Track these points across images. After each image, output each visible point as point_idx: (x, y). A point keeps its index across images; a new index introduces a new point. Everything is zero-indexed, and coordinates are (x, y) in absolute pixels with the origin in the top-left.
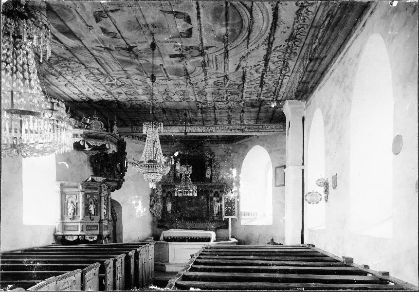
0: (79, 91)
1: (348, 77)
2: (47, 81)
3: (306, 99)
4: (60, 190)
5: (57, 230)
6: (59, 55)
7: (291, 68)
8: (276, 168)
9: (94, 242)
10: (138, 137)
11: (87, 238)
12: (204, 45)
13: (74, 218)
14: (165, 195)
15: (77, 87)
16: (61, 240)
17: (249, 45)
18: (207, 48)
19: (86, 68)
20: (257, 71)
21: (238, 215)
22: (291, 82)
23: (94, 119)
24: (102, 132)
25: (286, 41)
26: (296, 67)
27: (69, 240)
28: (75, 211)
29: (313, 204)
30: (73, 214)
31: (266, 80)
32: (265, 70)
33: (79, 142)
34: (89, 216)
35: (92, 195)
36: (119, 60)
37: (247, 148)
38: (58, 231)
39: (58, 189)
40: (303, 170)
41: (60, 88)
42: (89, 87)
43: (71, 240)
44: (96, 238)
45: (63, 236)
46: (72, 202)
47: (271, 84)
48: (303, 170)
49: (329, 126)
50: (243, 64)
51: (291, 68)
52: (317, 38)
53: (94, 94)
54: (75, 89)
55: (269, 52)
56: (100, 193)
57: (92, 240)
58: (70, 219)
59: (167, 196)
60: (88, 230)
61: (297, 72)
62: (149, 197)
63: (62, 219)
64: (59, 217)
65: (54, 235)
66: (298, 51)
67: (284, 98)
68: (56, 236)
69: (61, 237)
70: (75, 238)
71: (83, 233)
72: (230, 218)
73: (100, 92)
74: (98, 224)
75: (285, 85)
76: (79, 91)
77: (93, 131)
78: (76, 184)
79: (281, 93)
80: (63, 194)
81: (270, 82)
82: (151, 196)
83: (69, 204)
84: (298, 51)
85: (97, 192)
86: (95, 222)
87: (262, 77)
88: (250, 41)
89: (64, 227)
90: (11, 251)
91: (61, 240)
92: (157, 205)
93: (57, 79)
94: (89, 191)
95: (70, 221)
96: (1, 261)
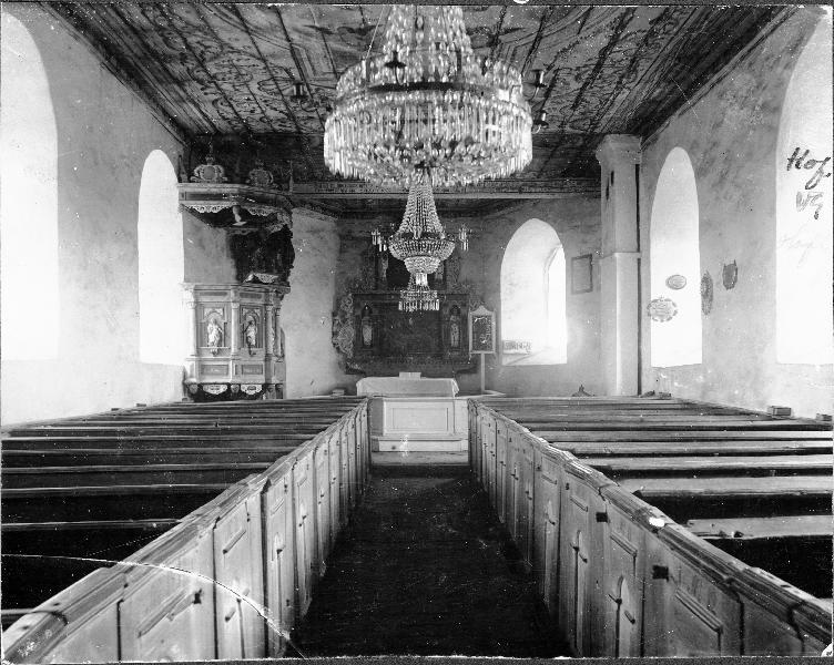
0: (236, 113)
1: (764, 88)
2: (182, 93)
3: (646, 135)
4: (193, 300)
5: (189, 372)
6: (227, 41)
7: (640, 74)
8: (574, 259)
9: (257, 396)
10: (311, 204)
11: (244, 388)
12: (503, 26)
13: (219, 352)
14: (359, 313)
15: (234, 105)
16: (198, 394)
17: (584, 28)
18: (507, 31)
19: (266, 68)
20: (577, 78)
21: (497, 347)
22: (633, 95)
23: (257, 167)
24: (272, 191)
25: (651, 22)
26: (649, 74)
27: (212, 392)
28: (223, 338)
29: (662, 321)
30: (219, 344)
31: (587, 96)
32: (592, 78)
33: (231, 209)
34: (247, 349)
35: (252, 308)
36: (334, 52)
37: (514, 225)
38: (191, 377)
39: (189, 296)
40: (639, 260)
41: (202, 105)
42: (256, 106)
43: (215, 392)
44: (259, 389)
45: (200, 386)
46: (216, 322)
47: (595, 101)
48: (639, 260)
49: (713, 176)
50: (559, 64)
51: (640, 74)
52: (706, 19)
53: (261, 119)
54: (229, 109)
55: (614, 41)
56: (266, 305)
57: (253, 393)
58: (214, 353)
59: (363, 315)
60: (246, 373)
61: (647, 82)
62: (330, 315)
63: (199, 352)
64: (192, 350)
65: (184, 384)
66: (663, 43)
67: (605, 131)
68: (186, 386)
69: (196, 387)
70: (223, 389)
71: (238, 381)
72: (483, 353)
73: (271, 114)
74: (263, 363)
75: (617, 104)
76: (236, 113)
77: (257, 190)
78: (223, 288)
79: (603, 122)
80: (198, 307)
81: (592, 101)
82: (334, 314)
83: (210, 325)
84: (663, 43)
85: (260, 302)
86: (259, 360)
87: (583, 89)
88: (588, 21)
89: (203, 369)
90: (29, 426)
91: (198, 394)
92: (345, 332)
93: (202, 89)
94: (247, 301)
95: (212, 357)
96: (4, 456)
